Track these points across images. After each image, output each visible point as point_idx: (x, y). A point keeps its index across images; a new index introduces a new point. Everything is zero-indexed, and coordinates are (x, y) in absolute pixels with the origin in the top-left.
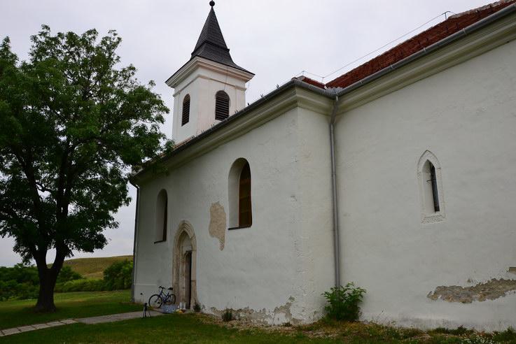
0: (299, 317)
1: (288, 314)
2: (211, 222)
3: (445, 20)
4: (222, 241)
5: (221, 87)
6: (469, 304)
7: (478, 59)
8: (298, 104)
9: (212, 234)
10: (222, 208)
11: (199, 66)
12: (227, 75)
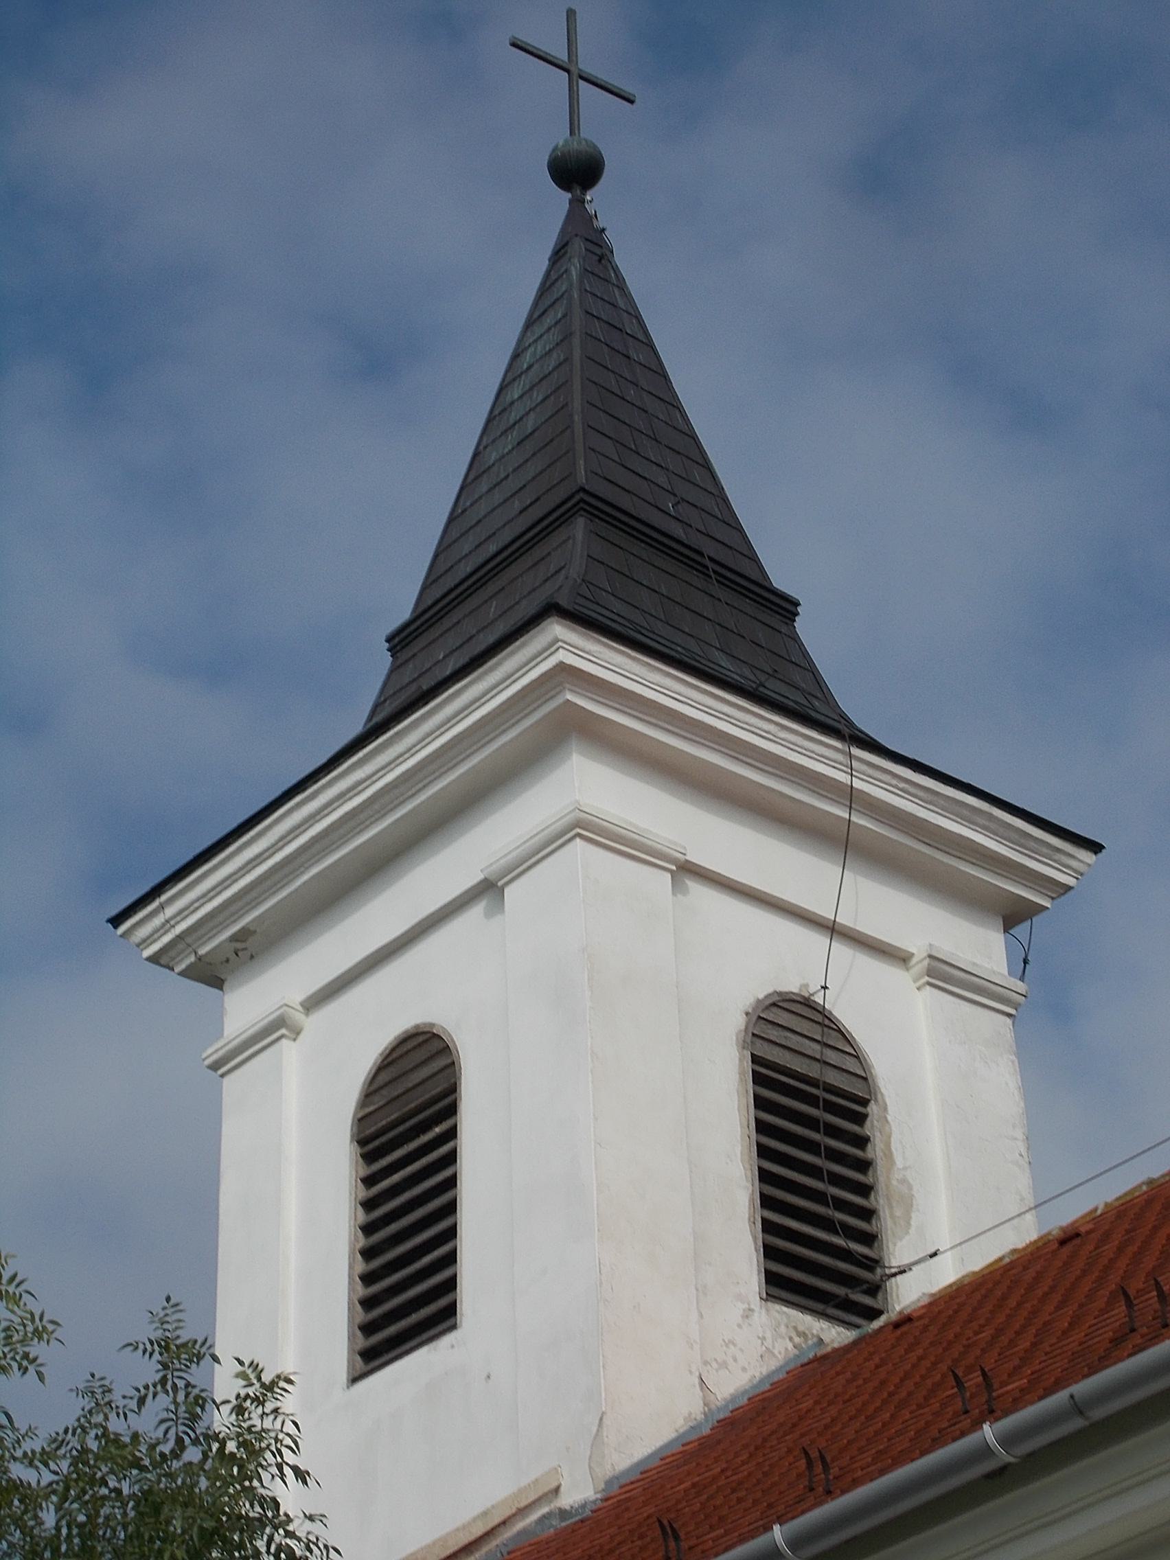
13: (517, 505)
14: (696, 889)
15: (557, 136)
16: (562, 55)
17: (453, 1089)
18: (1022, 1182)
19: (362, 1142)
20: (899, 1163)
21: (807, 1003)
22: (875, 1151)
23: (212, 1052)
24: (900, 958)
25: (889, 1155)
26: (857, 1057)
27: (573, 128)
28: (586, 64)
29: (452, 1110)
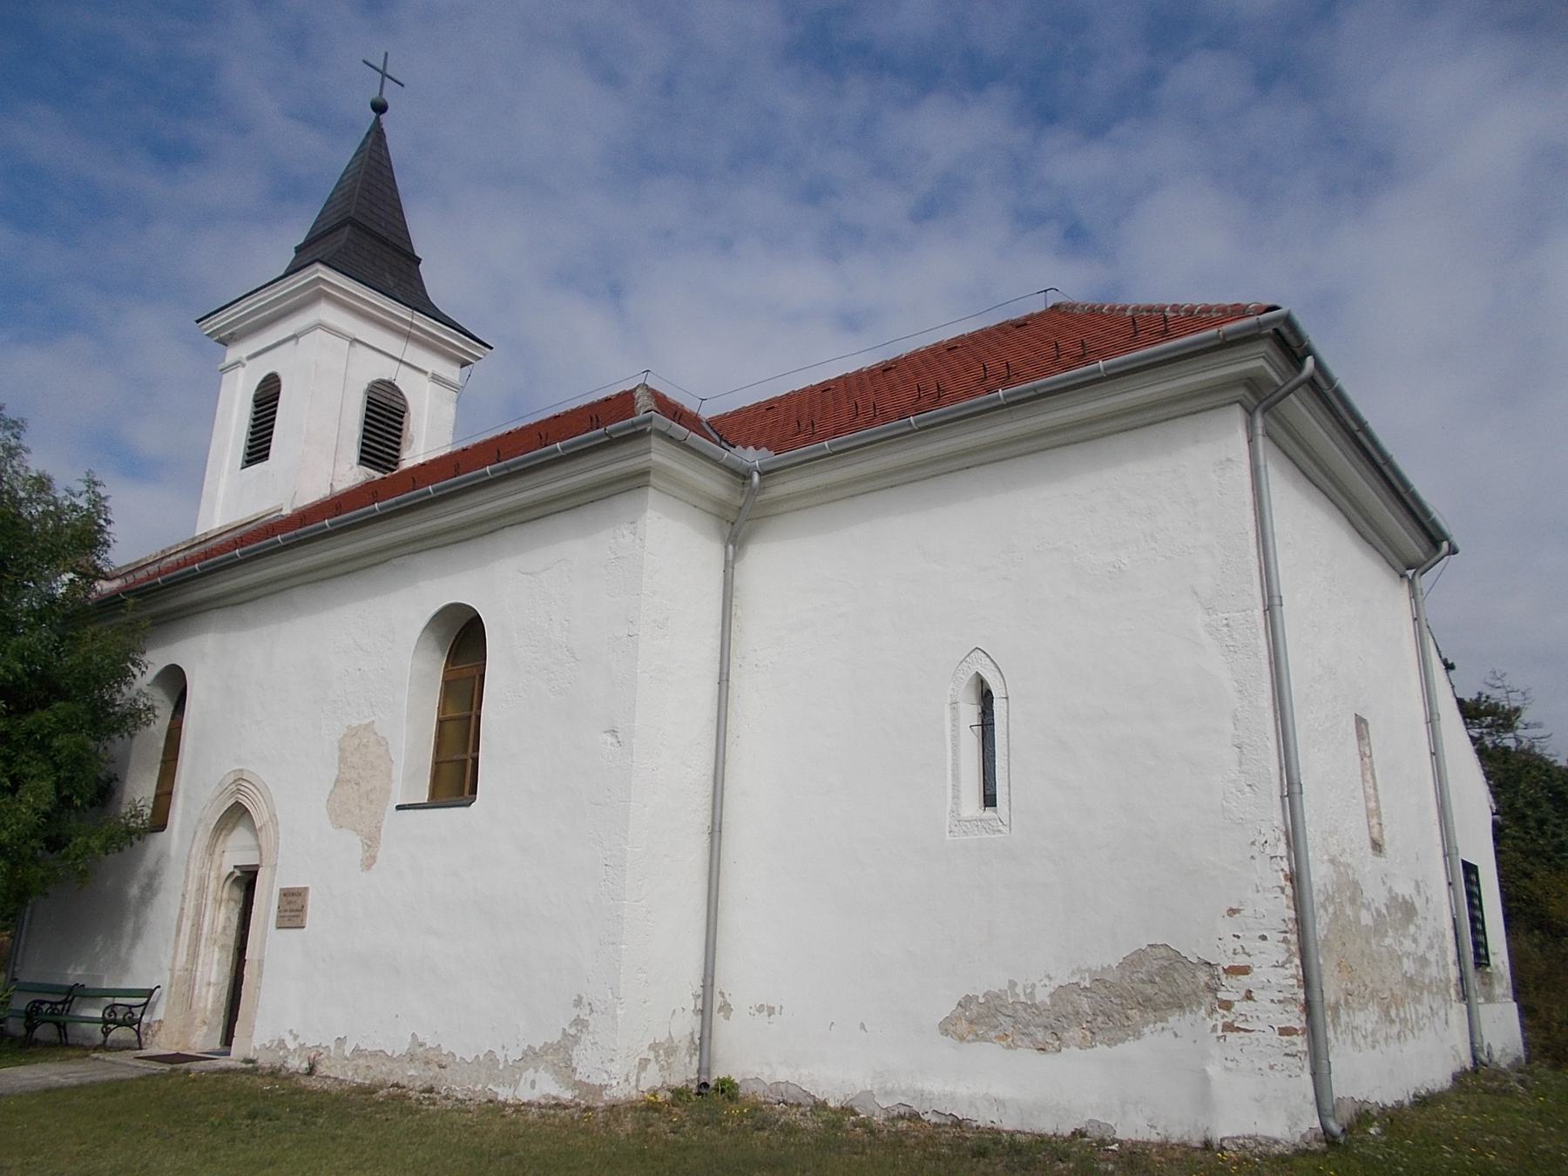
0: (601, 1079)
1: (565, 1069)
2: (338, 782)
3: (1044, 309)
4: (371, 842)
5: (385, 370)
6: (1013, 1051)
7: (1124, 438)
8: (653, 479)
9: (339, 815)
10: (382, 742)
11: (322, 295)
12: (408, 337)
13: (336, 216)
14: (358, 345)
15: (375, 94)
16: (381, 68)
17: (279, 393)
18: (449, 439)
19: (255, 401)
20: (411, 429)
21: (390, 383)
22: (404, 426)
23: (221, 366)
24: (425, 373)
25: (408, 428)
26: (404, 400)
27: (381, 93)
28: (389, 72)
29: (277, 399)
